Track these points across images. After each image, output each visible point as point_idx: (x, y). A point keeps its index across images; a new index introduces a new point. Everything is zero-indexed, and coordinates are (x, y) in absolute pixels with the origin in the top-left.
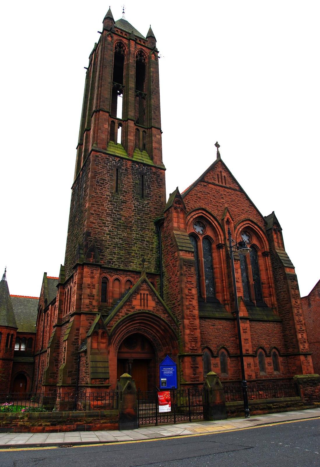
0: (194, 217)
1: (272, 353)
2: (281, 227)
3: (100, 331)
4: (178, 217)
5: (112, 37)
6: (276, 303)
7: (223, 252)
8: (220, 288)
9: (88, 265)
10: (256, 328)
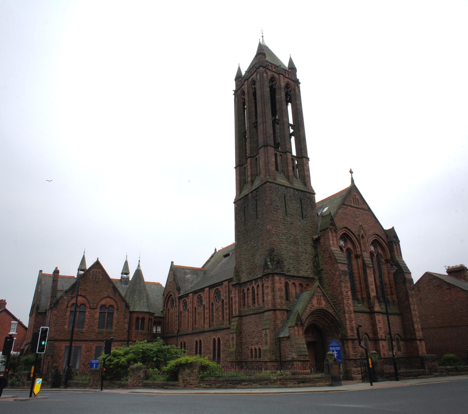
0: (340, 234)
1: (364, 338)
2: (399, 239)
3: (299, 323)
4: (333, 236)
5: (267, 73)
6: (396, 300)
7: (360, 261)
8: (359, 288)
9: (277, 274)
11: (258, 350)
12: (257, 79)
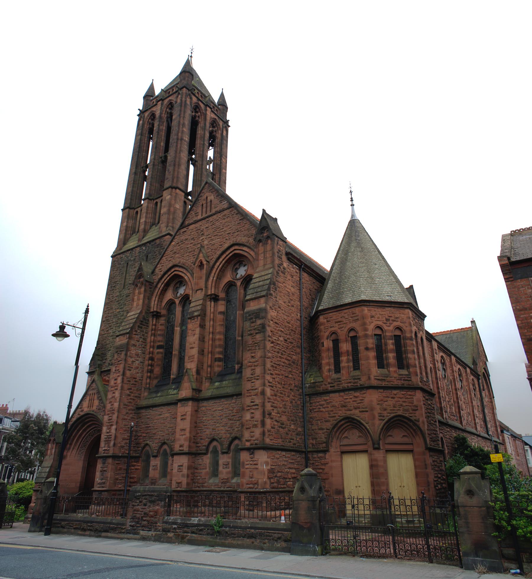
10: (213, 410)
11: (391, 344)
12: (176, 102)
